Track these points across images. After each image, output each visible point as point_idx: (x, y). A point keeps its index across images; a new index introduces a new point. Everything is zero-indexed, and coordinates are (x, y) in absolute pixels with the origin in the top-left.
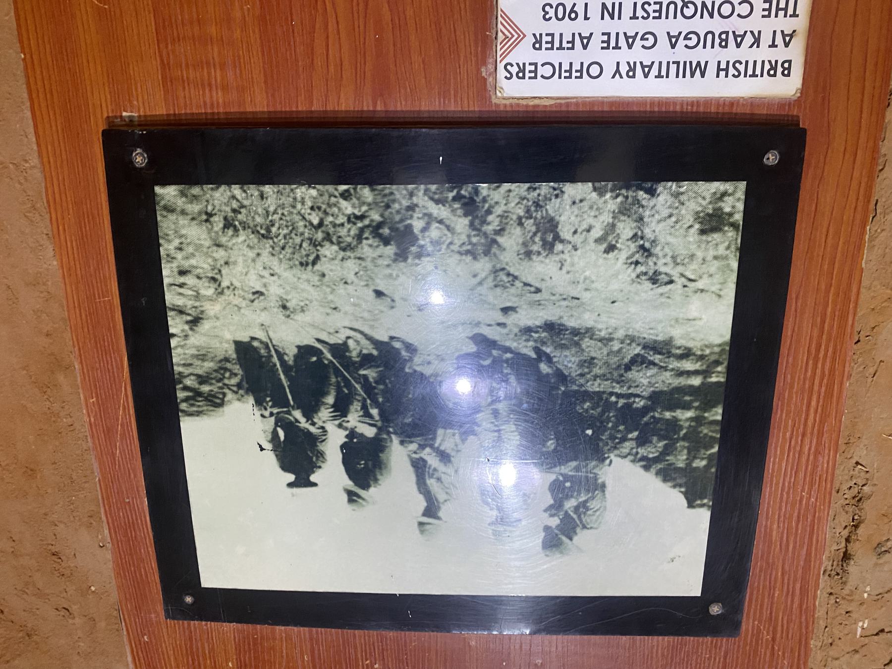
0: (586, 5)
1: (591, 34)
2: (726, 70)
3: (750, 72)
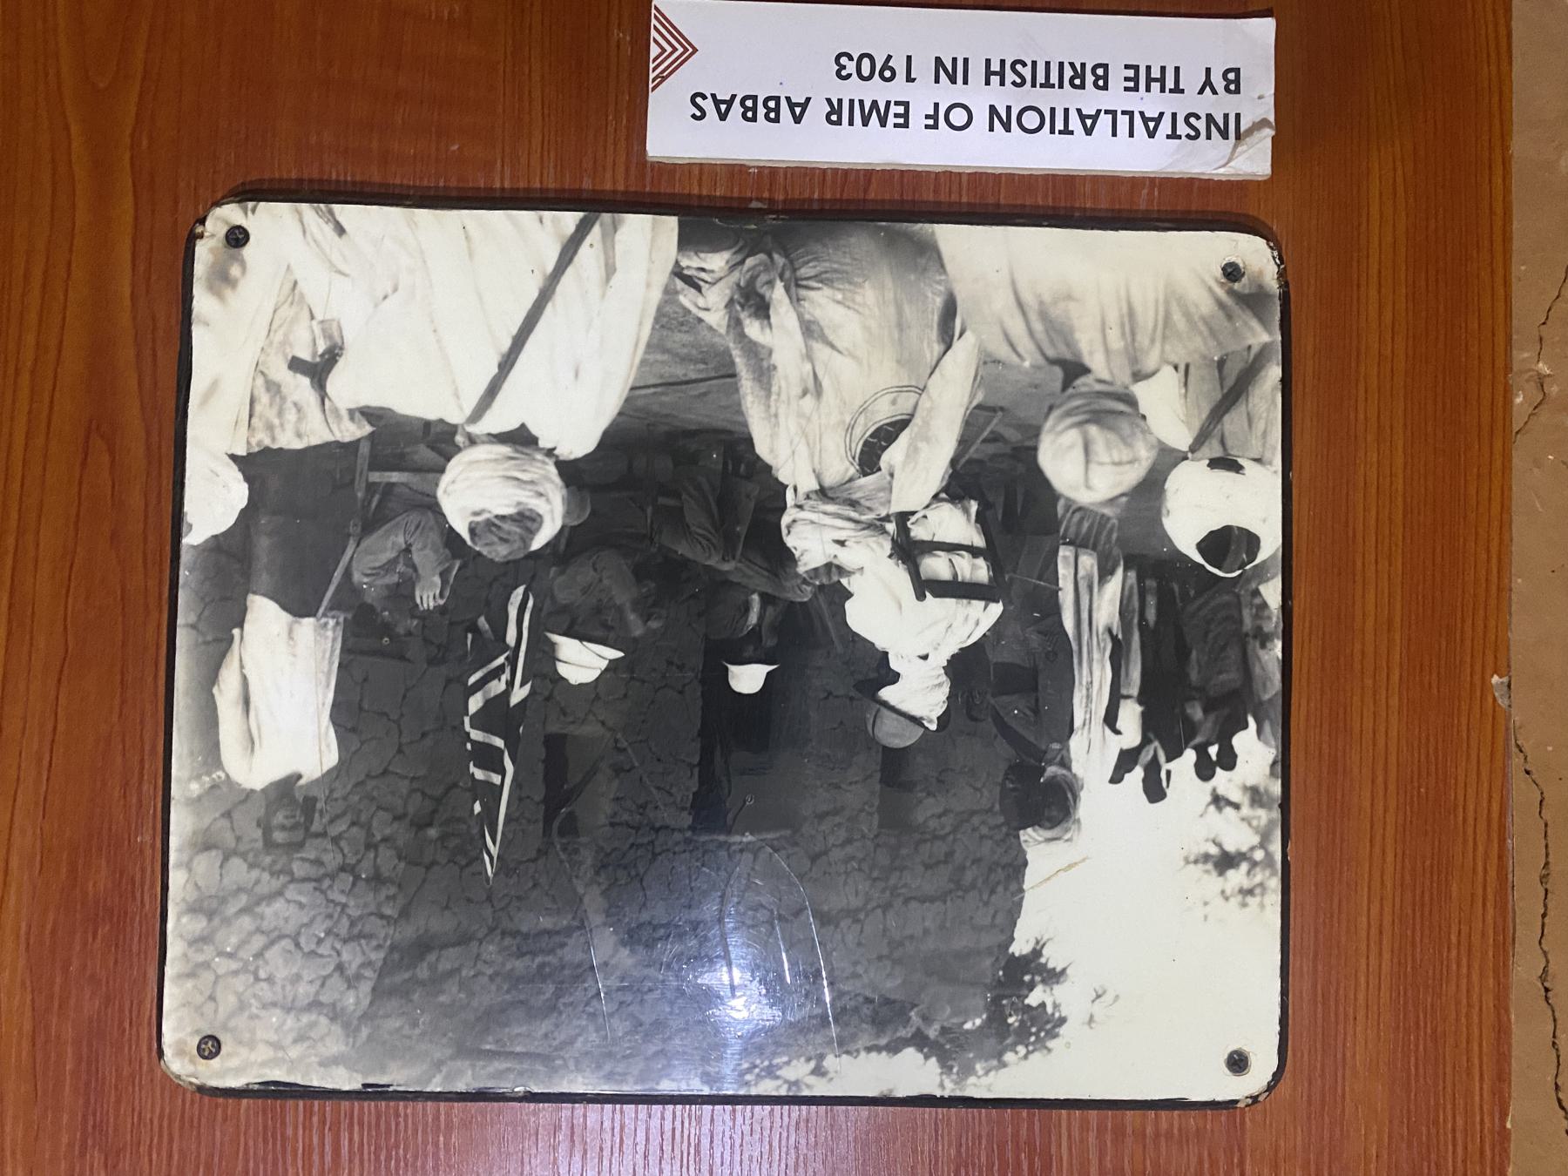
0: (909, 58)
1: (808, 100)
2: (1002, 74)
3: (1041, 79)
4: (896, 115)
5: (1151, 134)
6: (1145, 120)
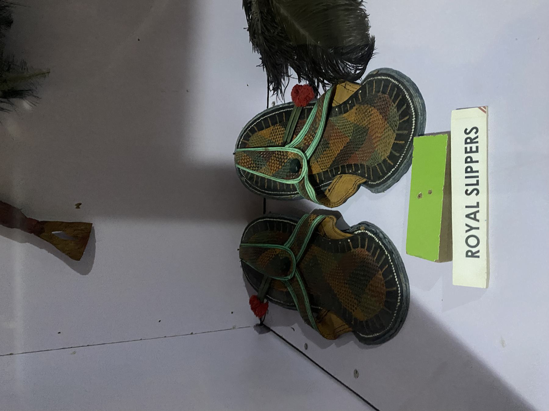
1: (478, 221)
4: (471, 148)
5: (468, 216)
6: (475, 213)
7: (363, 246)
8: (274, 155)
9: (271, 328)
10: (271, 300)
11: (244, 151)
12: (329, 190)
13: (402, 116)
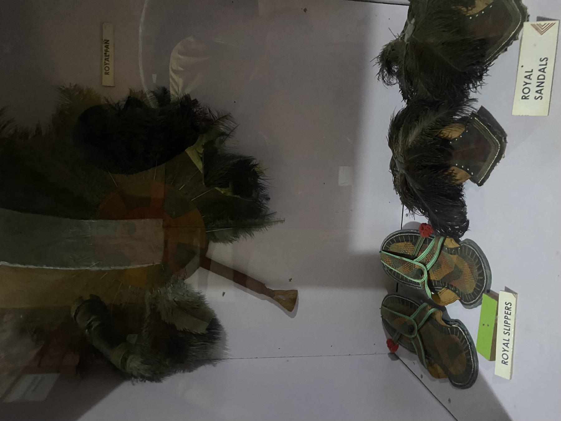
4: (508, 312)
7: (456, 335)
8: (407, 263)
9: (400, 357)
10: (401, 345)
11: (387, 255)
12: (440, 293)
13: (480, 275)
